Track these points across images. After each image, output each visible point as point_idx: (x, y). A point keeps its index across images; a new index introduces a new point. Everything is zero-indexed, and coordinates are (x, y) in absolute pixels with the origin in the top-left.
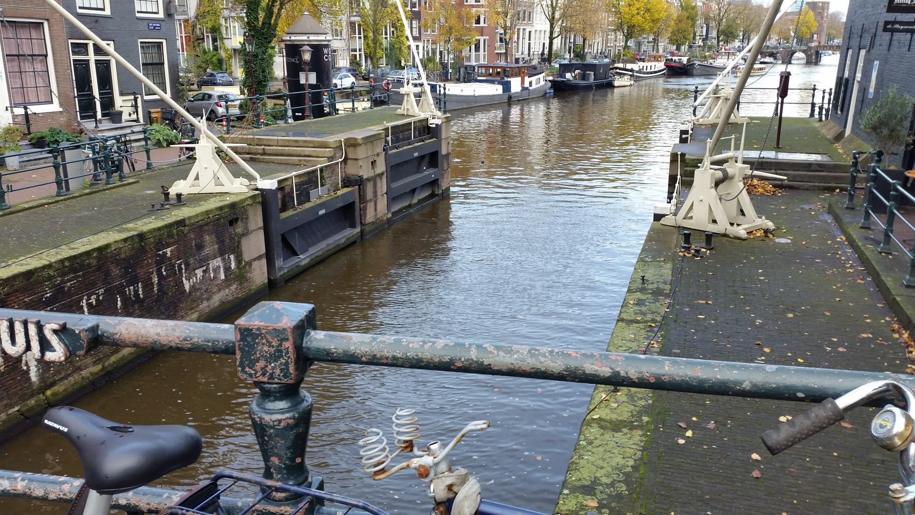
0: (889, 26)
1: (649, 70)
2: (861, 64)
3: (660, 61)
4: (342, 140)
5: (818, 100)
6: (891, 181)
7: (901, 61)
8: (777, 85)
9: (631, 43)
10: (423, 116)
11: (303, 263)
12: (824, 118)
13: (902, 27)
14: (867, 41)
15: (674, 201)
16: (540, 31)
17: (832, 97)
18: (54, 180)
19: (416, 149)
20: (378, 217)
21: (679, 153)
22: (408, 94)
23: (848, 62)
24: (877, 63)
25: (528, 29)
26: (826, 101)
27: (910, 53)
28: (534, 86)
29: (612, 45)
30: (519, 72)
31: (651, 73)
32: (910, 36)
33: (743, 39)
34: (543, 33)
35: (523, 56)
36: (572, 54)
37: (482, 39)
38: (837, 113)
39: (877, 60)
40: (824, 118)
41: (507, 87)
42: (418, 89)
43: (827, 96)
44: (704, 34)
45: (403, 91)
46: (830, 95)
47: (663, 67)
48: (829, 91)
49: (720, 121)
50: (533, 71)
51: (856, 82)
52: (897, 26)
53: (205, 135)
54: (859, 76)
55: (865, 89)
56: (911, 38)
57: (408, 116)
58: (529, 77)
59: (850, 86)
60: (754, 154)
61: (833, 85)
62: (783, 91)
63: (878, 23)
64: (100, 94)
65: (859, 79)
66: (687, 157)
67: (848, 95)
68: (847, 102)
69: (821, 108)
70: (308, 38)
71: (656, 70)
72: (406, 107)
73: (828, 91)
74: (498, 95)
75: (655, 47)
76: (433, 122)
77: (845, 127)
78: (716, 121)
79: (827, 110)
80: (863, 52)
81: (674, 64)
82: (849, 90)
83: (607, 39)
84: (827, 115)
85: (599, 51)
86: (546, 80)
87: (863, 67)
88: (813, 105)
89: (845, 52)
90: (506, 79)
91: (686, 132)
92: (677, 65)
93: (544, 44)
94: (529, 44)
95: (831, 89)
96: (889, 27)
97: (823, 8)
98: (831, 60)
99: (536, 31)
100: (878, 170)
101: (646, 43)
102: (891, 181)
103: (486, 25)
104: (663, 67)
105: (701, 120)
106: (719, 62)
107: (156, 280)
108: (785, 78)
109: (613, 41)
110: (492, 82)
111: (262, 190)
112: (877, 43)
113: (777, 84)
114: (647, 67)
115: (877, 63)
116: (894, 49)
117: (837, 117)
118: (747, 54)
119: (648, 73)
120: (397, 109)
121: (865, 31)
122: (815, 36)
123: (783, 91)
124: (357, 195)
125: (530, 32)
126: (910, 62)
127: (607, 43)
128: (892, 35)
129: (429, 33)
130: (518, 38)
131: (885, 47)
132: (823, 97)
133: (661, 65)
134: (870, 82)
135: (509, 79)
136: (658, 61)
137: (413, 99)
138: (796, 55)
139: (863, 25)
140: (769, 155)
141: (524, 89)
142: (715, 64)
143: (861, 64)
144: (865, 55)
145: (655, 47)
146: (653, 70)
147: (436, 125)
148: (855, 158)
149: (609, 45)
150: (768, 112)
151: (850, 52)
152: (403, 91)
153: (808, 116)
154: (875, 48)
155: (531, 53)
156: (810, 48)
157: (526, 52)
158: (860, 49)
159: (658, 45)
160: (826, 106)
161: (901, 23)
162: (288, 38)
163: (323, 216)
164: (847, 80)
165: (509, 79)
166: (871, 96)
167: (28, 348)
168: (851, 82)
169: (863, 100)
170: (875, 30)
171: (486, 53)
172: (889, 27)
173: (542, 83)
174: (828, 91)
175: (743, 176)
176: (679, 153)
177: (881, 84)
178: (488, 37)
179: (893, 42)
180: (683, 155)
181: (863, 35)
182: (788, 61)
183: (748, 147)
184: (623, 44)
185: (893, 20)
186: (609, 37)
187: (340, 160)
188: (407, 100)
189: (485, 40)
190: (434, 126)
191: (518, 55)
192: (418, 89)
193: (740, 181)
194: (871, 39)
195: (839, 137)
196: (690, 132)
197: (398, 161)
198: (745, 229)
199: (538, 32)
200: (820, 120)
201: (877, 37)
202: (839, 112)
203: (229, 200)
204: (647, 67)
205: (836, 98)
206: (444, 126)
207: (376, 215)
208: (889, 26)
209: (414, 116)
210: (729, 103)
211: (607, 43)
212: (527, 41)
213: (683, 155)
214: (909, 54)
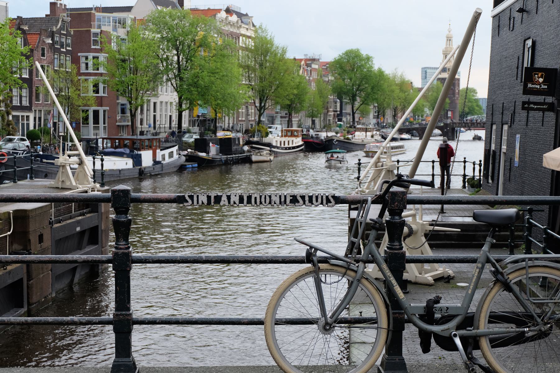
0: (526, 106)
1: (286, 146)
2: (505, 138)
3: (297, 136)
7: (537, 134)
13: (536, 107)
14: (508, 118)
16: (166, 103)
17: (482, 168)
19: (78, 222)
23: (493, 137)
24: (518, 136)
25: (153, 100)
26: (477, 173)
27: (544, 127)
28: (167, 160)
29: (244, 119)
30: (149, 146)
31: (290, 148)
32: (542, 114)
33: (378, 115)
34: (169, 104)
37: (101, 110)
38: (488, 182)
39: (518, 133)
41: (137, 160)
43: (477, 167)
44: (338, 109)
46: (480, 165)
47: (301, 143)
48: (479, 162)
50: (164, 145)
51: (502, 153)
52: (532, 106)
55: (511, 159)
56: (543, 115)
58: (161, 150)
59: (497, 157)
63: (515, 102)
65: (505, 151)
67: (497, 165)
71: (294, 145)
72: (60, 180)
73: (479, 163)
74: (129, 169)
80: (506, 127)
81: (311, 140)
82: (497, 161)
85: (231, 125)
86: (180, 154)
87: (508, 139)
89: (490, 127)
90: (136, 152)
92: (316, 141)
93: (171, 116)
94: (155, 116)
95: (480, 161)
96: (526, 107)
99: (161, 102)
100: (531, 220)
101: (279, 117)
103: (106, 95)
104: (301, 143)
109: (244, 115)
110: (121, 155)
112: (517, 119)
114: (284, 142)
115: (518, 136)
116: (531, 124)
117: (489, 186)
119: (286, 149)
121: (505, 109)
124: (25, 271)
125: (155, 103)
126: (544, 135)
128: (528, 113)
129: (41, 102)
131: (524, 123)
132: (474, 169)
133: (298, 141)
134: (515, 152)
135: (139, 152)
136: (295, 136)
139: (503, 103)
141: (156, 162)
142: (353, 140)
144: (508, 129)
146: (291, 145)
149: (240, 119)
151: (494, 127)
154: (515, 123)
155: (157, 126)
161: (535, 104)
164: (494, 152)
165: (139, 152)
166: (516, 165)
168: (498, 154)
169: (510, 169)
170: (513, 108)
171: (106, 125)
172: (526, 107)
173: (176, 156)
175: (424, 232)
177: (524, 154)
178: (108, 108)
179: (529, 119)
181: (504, 112)
185: (527, 100)
186: (240, 110)
187: (9, 233)
188: (62, 172)
189: (104, 111)
191: (145, 126)
193: (422, 236)
194: (512, 116)
197: (62, 235)
199: (164, 104)
201: (516, 114)
202: (490, 181)
204: (284, 142)
208: (526, 106)
209: (70, 189)
211: (238, 117)
212: (152, 114)
214: (543, 129)
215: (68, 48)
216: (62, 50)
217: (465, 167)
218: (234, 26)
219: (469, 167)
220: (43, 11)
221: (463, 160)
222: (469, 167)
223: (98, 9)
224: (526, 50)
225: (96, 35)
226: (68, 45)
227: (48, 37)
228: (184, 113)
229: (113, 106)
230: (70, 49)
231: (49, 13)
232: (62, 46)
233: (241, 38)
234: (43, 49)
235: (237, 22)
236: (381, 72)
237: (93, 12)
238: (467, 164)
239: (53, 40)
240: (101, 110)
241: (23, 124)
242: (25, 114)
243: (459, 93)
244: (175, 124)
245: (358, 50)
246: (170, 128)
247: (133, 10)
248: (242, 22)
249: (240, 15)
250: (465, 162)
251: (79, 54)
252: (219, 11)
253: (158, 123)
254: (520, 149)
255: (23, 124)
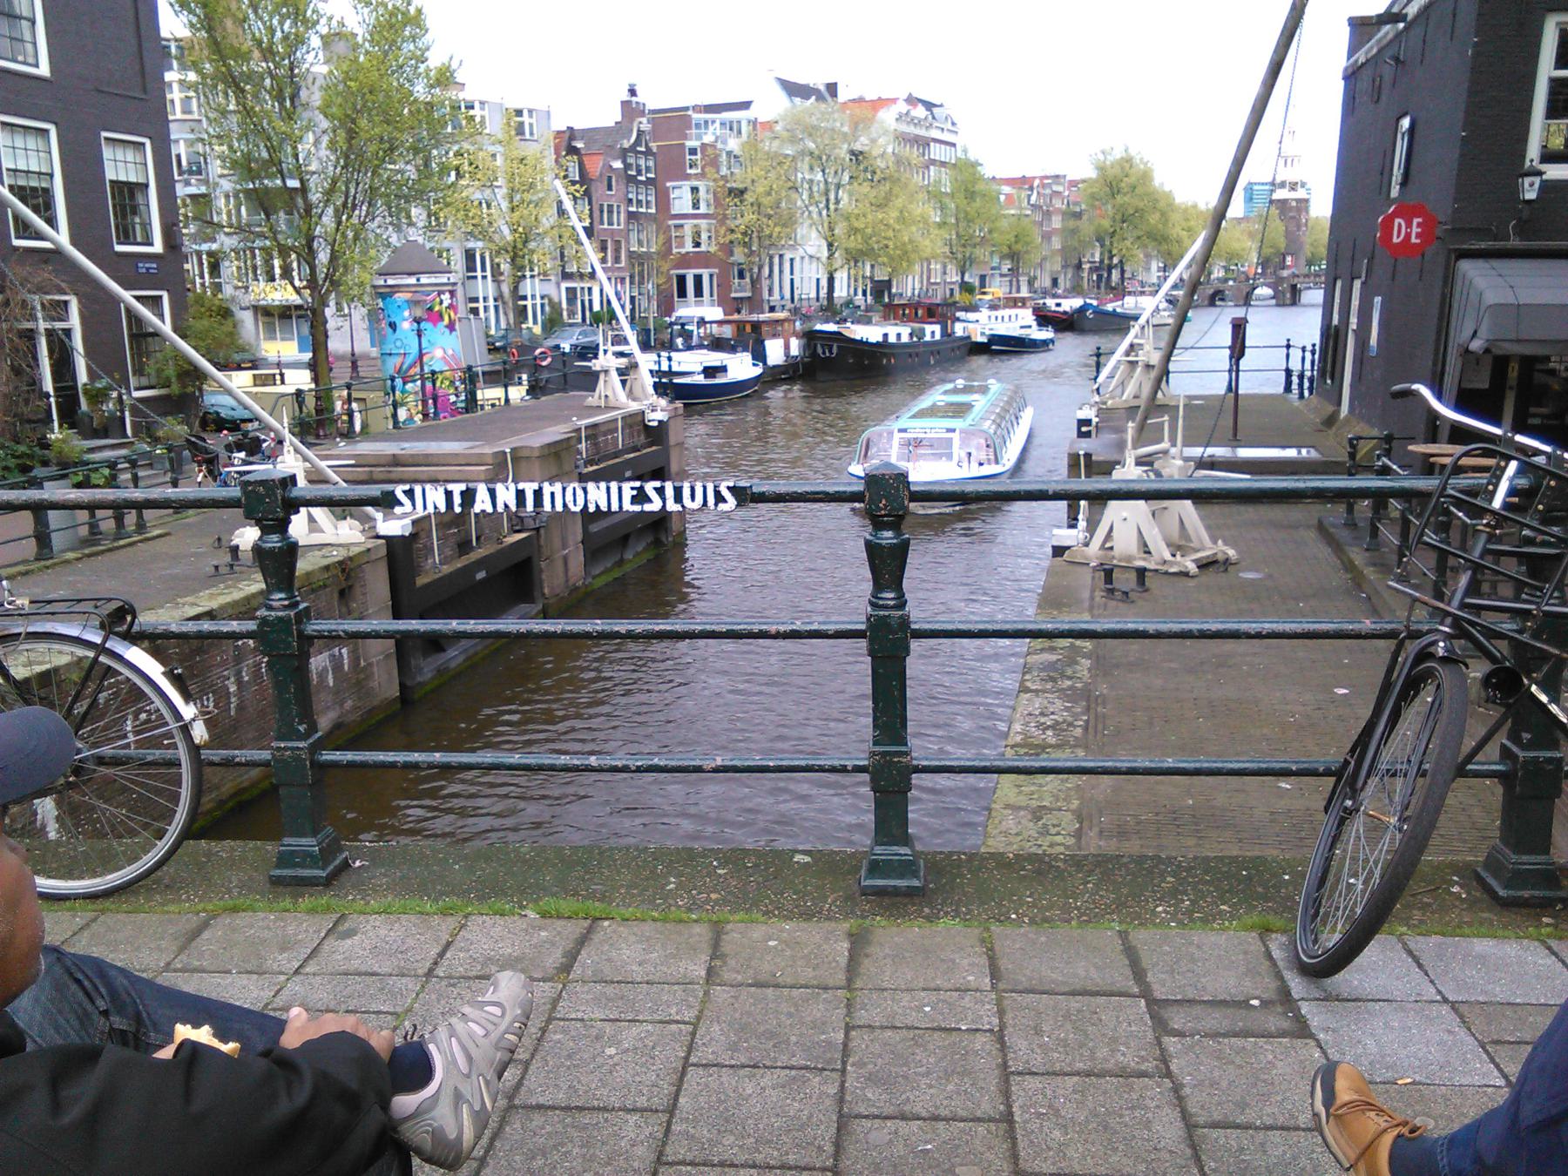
2: (1355, 303)
4: (508, 450)
5: (1295, 365)
6: (1469, 521)
8: (1229, 342)
9: (971, 276)
10: (634, 406)
11: (453, 665)
12: (1306, 393)
15: (1082, 524)
17: (1317, 356)
18: (31, 533)
20: (571, 582)
21: (1082, 453)
22: (606, 372)
23: (1337, 300)
24: (1378, 300)
26: (1308, 365)
35: (783, 303)
36: (869, 298)
40: (1306, 393)
42: (623, 361)
43: (1308, 356)
45: (596, 365)
46: (1313, 353)
49: (1142, 402)
53: (291, 449)
54: (1354, 320)
57: (608, 408)
60: (1197, 452)
61: (1317, 340)
62: (1238, 349)
64: (56, 389)
66: (1094, 458)
68: (1339, 358)
69: (1301, 377)
70: (418, 280)
75: (1014, 283)
76: (654, 418)
77: (1339, 404)
78: (1135, 403)
79: (1311, 380)
80: (1357, 284)
83: (929, 270)
84: (1311, 389)
85: (916, 292)
88: (1288, 372)
91: (1088, 422)
94: (792, 280)
95: (1314, 345)
97: (1299, 210)
98: (1315, 296)
102: (1469, 521)
105: (1110, 402)
106: (1129, 304)
107: (233, 689)
108: (1239, 328)
111: (389, 539)
113: (1227, 339)
115: (1378, 300)
118: (1174, 293)
120: (587, 397)
122: (1289, 259)
123: (1238, 349)
125: (792, 260)
127: (929, 278)
130: (771, 271)
132: (1303, 359)
137: (615, 379)
138: (1258, 291)
140: (1220, 452)
143: (1355, 303)
145: (1014, 283)
147: (660, 422)
148: (1352, 446)
149: (932, 280)
150: (1217, 385)
151: (1339, 284)
152: (596, 365)
153: (1281, 389)
155: (796, 297)
156: (1282, 279)
157: (787, 295)
158: (1353, 279)
159: (1018, 281)
160: (1308, 374)
162: (382, 283)
163: (482, 581)
167: (705, 503)
168: (1342, 333)
174: (1309, 348)
176: (1082, 453)
178: (717, 271)
180: (1088, 456)
182: (1247, 300)
183: (1188, 443)
184: (959, 278)
189: (711, 276)
190: (655, 424)
192: (623, 361)
195: (1331, 421)
196: (1095, 420)
198: (1193, 561)
200: (1301, 396)
202: (1329, 381)
203: (337, 555)
205: (1323, 358)
206: (672, 423)
207: (567, 581)
209: (619, 409)
210: (1154, 374)
211: (929, 278)
213: (1088, 456)
215: (649, 175)
216: (639, 178)
217: (1288, 356)
218: (921, 126)
219: (1296, 354)
220: (609, 116)
221: (1285, 343)
222: (1296, 354)
223: (697, 109)
224: (1399, 136)
225: (693, 151)
226: (648, 169)
227: (615, 159)
228: (837, 275)
229: (725, 267)
230: (652, 176)
231: (619, 119)
232: (639, 172)
233: (932, 144)
234: (610, 178)
235: (926, 118)
236: (1169, 196)
237: (690, 113)
238: (1291, 350)
239: (624, 162)
240: (705, 273)
241: (583, 302)
242: (586, 285)
243: (1306, 225)
244: (824, 292)
245: (1128, 161)
246: (818, 299)
247: (753, 106)
248: (934, 118)
249: (929, 106)
250: (1288, 346)
251: (668, 184)
252: (894, 101)
253: (796, 293)
254: (50, 877)
255: (583, 302)
